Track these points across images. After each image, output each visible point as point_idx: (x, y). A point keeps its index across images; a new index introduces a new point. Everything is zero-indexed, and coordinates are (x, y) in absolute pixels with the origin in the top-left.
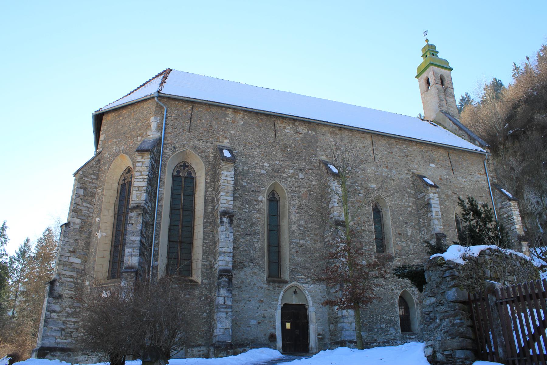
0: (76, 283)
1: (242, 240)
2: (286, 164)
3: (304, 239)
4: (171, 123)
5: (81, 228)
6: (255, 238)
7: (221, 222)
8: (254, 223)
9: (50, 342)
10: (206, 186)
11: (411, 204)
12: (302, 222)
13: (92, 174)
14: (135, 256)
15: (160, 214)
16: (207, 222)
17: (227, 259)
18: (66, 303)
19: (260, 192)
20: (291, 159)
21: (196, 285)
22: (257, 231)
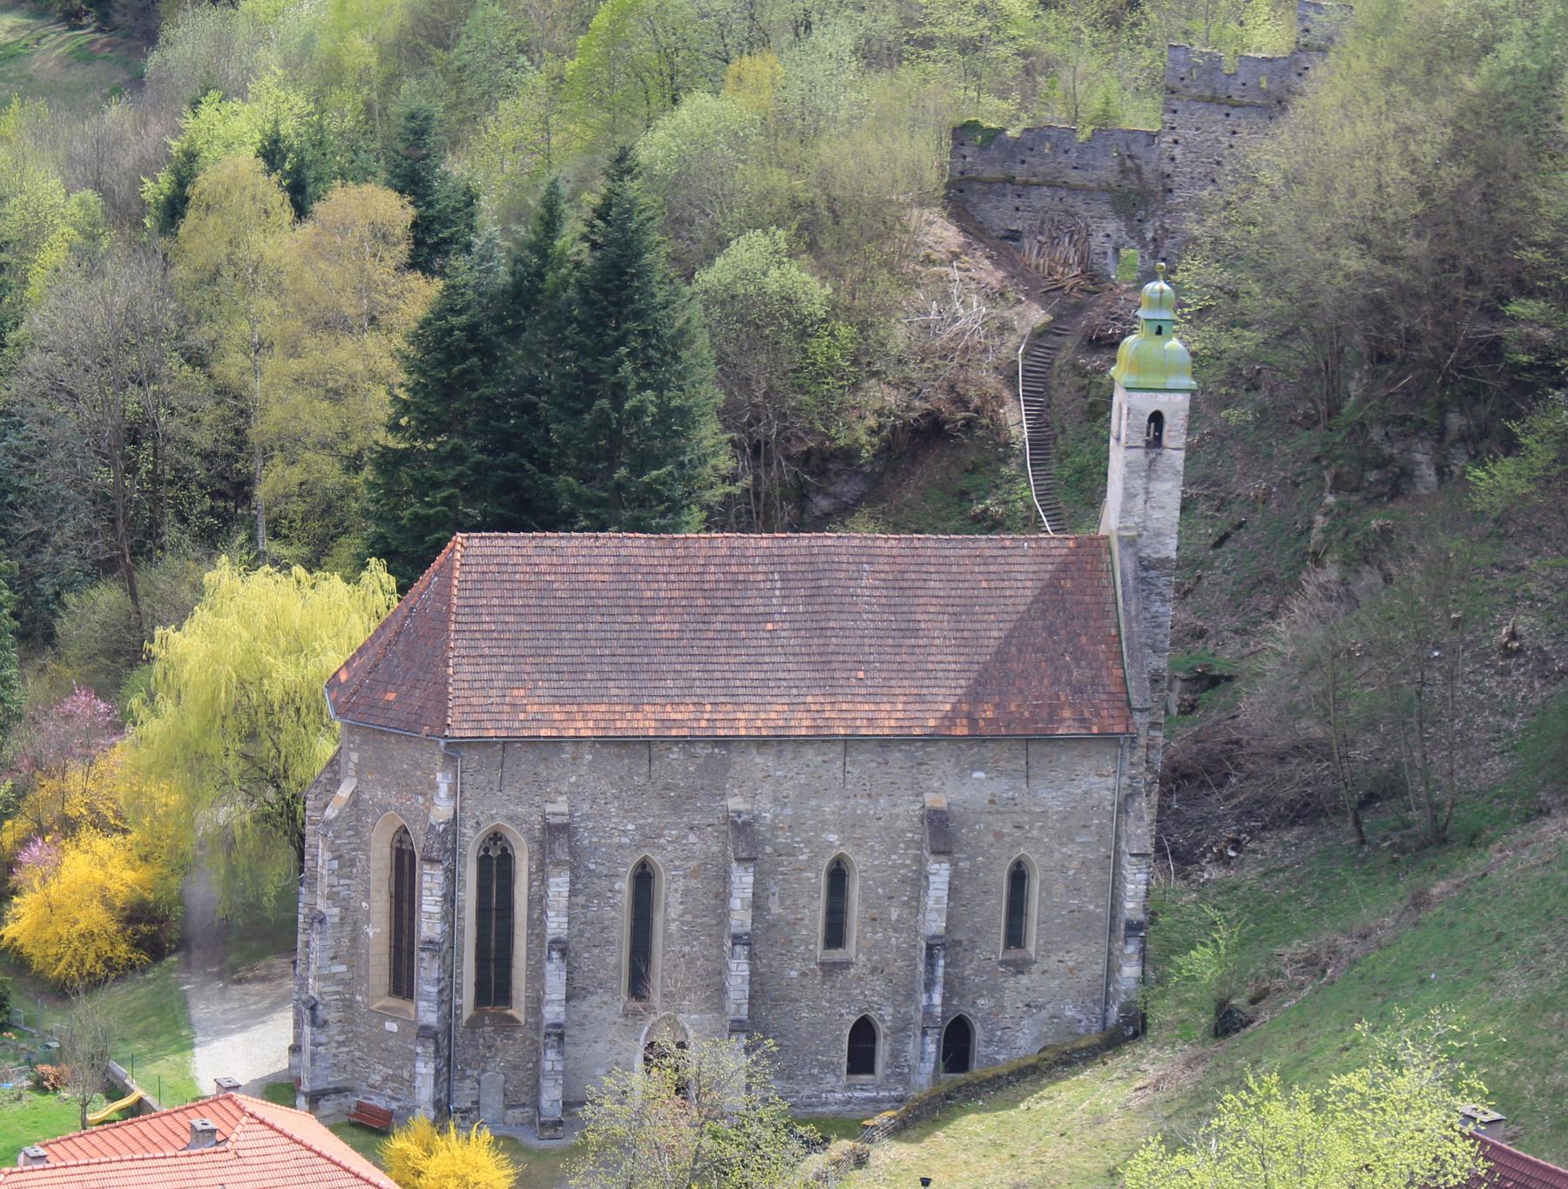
4: (470, 780)
5: (342, 919)
9: (320, 1085)
12: (688, 918)
15: (462, 931)
17: (557, 1009)
18: (333, 1030)
20: (675, 808)
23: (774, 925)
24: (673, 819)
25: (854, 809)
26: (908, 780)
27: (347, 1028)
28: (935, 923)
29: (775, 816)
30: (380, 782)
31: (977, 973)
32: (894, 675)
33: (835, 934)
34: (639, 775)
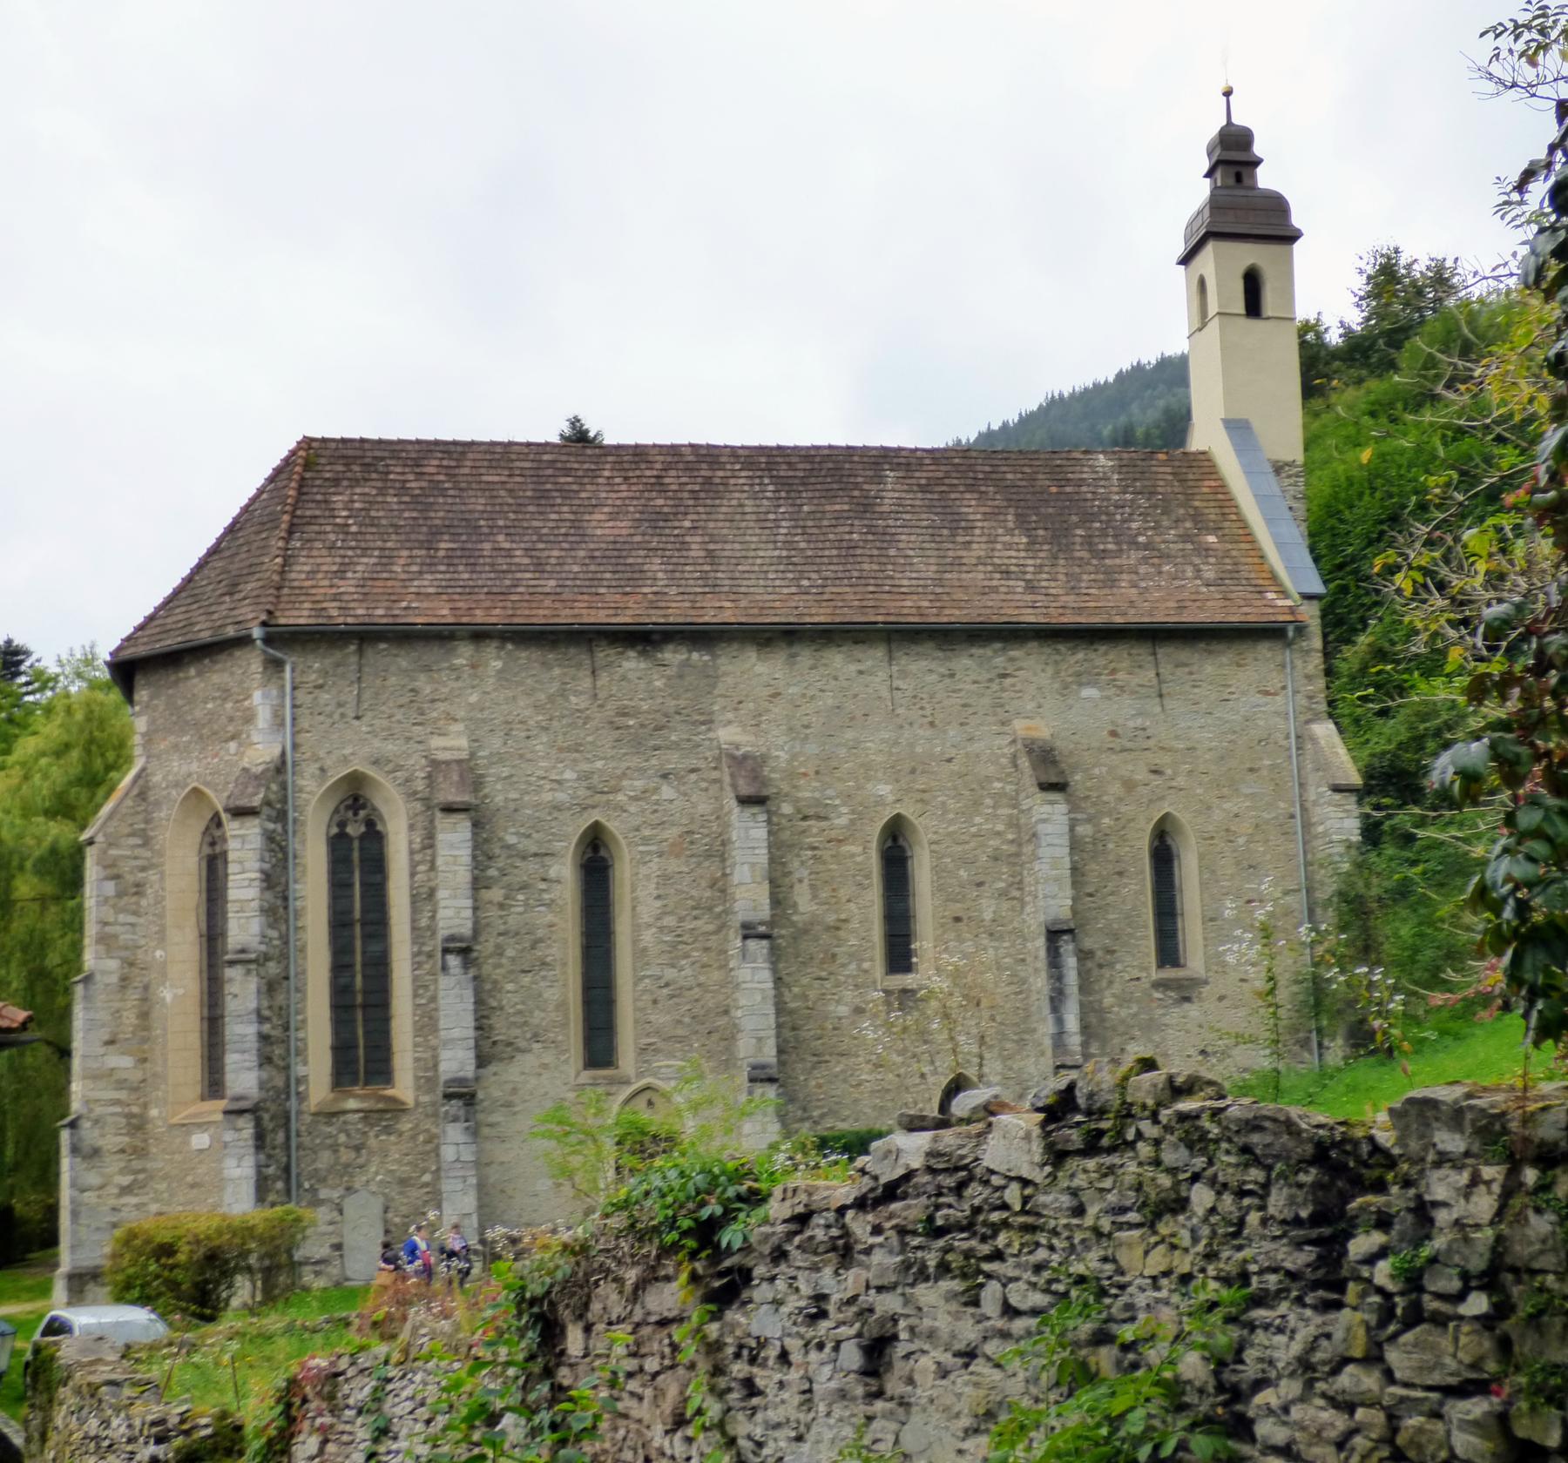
0: (130, 1116)
1: (510, 987)
2: (624, 765)
3: (673, 966)
6: (544, 978)
7: (445, 968)
8: (541, 940)
10: (412, 860)
11: (1000, 827)
12: (669, 921)
13: (129, 835)
14: (249, 1069)
16: (419, 953)
18: (113, 1165)
19: (552, 855)
21: (403, 1111)
22: (549, 959)
23: (806, 932)
24: (635, 761)
25: (911, 745)
26: (986, 701)
27: (136, 1164)
28: (1057, 903)
29: (794, 757)
30: (176, 747)
31: (1124, 1000)
32: (948, 568)
33: (899, 955)
34: (577, 693)
